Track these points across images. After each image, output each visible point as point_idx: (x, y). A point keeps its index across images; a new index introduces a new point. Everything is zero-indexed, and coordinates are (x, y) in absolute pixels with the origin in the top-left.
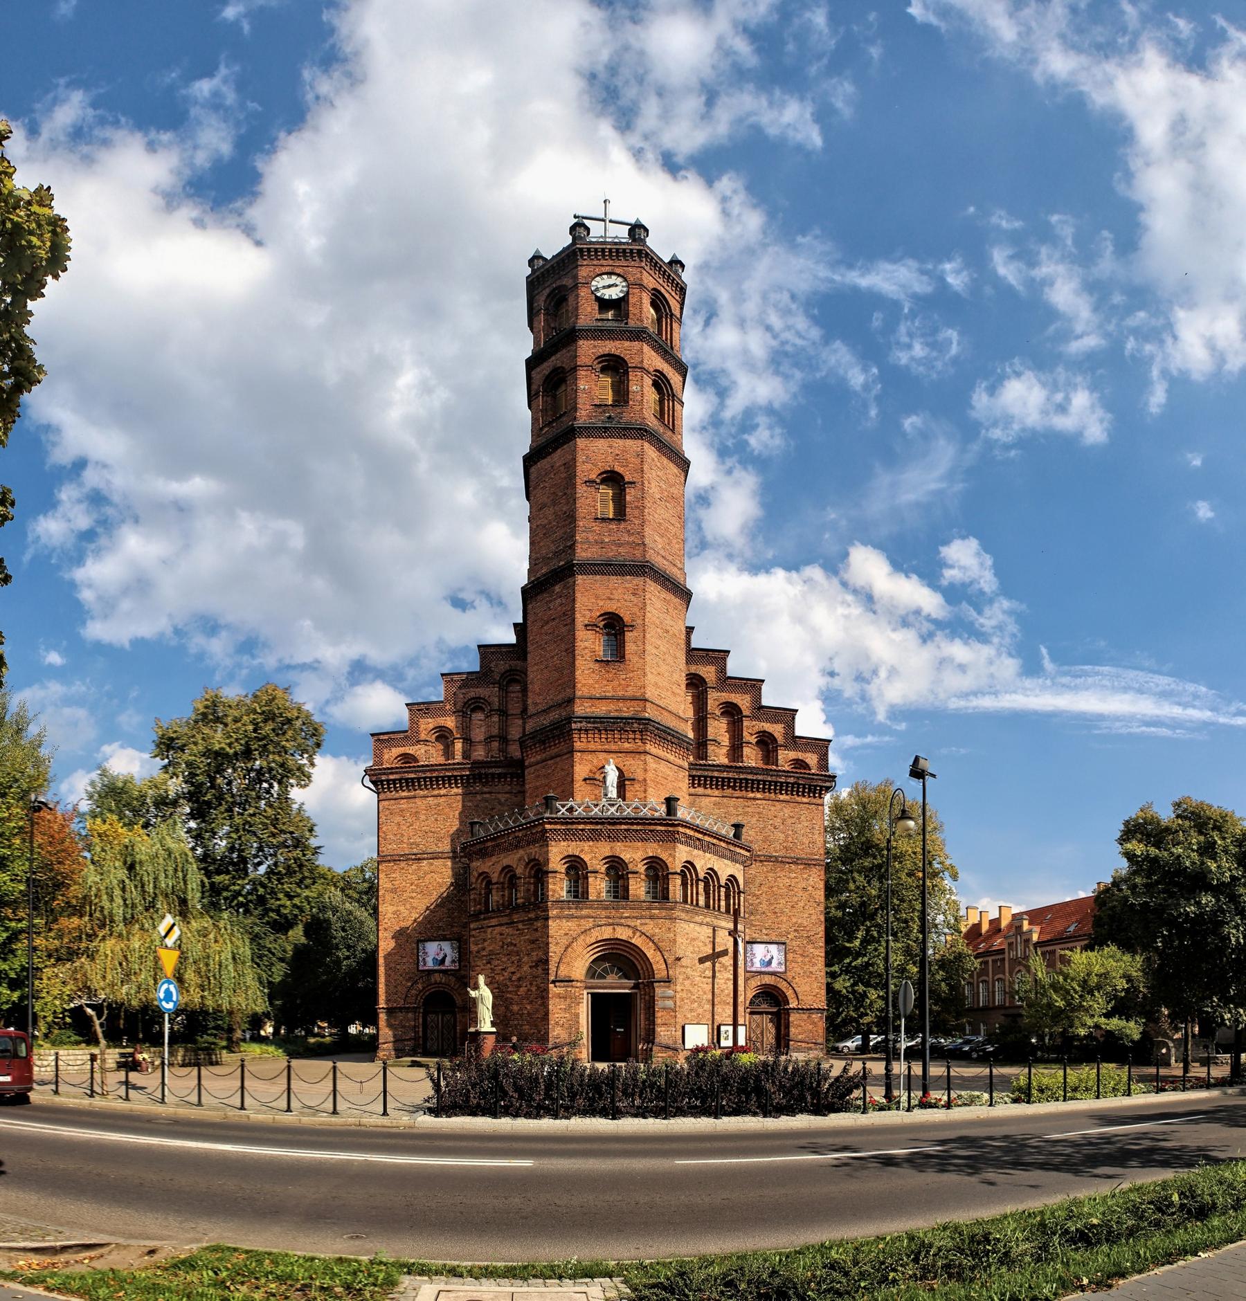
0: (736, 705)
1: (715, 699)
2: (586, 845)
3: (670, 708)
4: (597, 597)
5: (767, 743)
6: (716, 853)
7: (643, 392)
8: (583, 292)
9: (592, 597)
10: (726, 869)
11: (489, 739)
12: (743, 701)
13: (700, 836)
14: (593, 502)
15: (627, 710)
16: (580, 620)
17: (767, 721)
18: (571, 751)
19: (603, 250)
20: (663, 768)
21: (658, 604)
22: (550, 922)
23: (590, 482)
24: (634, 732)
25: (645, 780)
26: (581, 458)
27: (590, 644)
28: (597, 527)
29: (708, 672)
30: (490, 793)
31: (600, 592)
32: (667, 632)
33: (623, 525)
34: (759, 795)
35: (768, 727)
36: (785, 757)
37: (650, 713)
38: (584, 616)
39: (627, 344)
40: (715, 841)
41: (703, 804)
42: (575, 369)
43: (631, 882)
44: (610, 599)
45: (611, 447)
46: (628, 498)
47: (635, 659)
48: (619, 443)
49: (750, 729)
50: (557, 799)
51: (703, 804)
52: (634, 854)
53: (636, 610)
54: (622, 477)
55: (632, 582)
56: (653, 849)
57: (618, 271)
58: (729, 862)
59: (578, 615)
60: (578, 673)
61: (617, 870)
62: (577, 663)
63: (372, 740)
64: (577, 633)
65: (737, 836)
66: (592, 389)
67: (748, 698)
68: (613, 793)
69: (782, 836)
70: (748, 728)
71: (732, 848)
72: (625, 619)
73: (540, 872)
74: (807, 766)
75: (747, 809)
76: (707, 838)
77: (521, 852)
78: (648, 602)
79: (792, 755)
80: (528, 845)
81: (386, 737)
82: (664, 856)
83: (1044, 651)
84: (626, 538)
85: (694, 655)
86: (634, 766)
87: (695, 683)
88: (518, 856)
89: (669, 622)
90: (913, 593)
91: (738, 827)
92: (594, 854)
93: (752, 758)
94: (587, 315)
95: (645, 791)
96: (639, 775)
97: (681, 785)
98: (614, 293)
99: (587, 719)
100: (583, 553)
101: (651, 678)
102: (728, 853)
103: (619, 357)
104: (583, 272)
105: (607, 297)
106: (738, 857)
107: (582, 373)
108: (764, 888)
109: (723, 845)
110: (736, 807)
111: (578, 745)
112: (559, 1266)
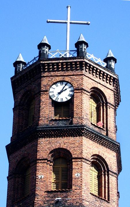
8: (44, 98)
57: (67, 79)
66: (46, 177)
94: (47, 114)
98: (65, 97)
103: (66, 150)
104: (45, 82)
105: (59, 101)
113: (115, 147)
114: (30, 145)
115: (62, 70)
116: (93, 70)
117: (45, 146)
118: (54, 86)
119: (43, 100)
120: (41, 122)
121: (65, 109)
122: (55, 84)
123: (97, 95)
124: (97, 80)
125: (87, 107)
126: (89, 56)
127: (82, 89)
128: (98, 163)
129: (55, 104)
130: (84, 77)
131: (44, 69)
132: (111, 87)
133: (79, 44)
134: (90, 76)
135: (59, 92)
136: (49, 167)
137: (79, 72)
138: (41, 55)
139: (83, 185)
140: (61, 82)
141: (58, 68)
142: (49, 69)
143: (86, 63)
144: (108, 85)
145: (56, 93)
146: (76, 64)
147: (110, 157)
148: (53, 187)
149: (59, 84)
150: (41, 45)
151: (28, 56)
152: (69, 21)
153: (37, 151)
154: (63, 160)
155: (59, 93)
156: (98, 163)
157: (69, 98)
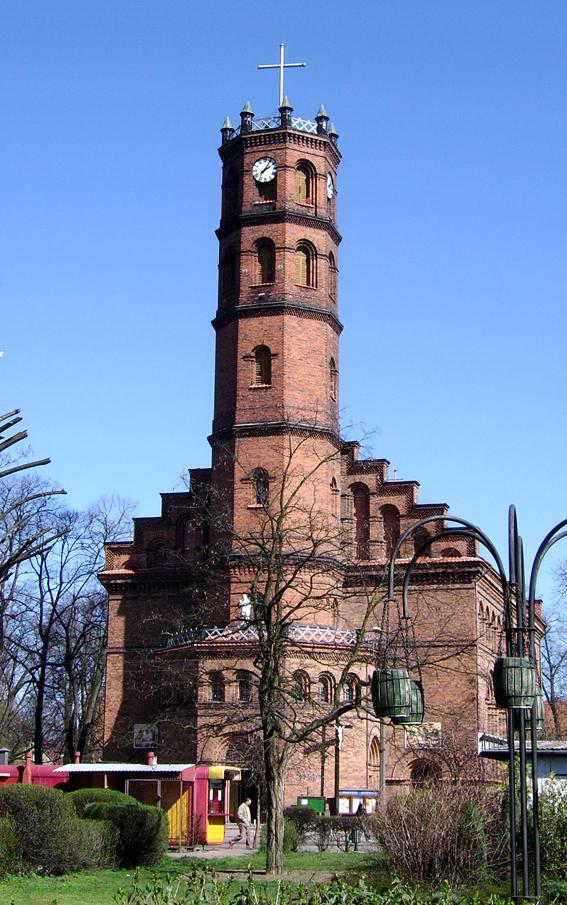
1: (376, 503)
5: (423, 545)
7: (292, 266)
8: (247, 179)
14: (248, 373)
16: (239, 474)
22: (198, 719)
23: (247, 357)
28: (251, 395)
29: (370, 480)
39: (275, 226)
44: (259, 457)
45: (261, 323)
48: (267, 320)
49: (407, 525)
50: (206, 628)
55: (274, 440)
57: (270, 154)
66: (251, 270)
67: (403, 497)
70: (404, 525)
79: (443, 545)
83: (131, 572)
85: (354, 467)
87: (360, 492)
90: (45, 620)
94: (252, 198)
98: (268, 176)
103: (269, 238)
104: (247, 159)
105: (263, 181)
112: (178, 838)
113: (328, 226)
114: (234, 234)
115: (265, 144)
116: (298, 138)
117: (249, 235)
118: (257, 163)
119: (246, 181)
120: (244, 209)
121: (269, 189)
122: (258, 160)
123: (305, 166)
124: (305, 149)
125: (294, 181)
126: (300, 124)
127: (286, 166)
128: (306, 247)
129: (259, 184)
130: (288, 151)
131: (246, 144)
132: (322, 153)
133: (283, 110)
134: (296, 147)
135: (263, 171)
136: (255, 258)
137: (281, 145)
138: (244, 126)
139: (287, 277)
140: (265, 158)
141: (260, 142)
142: (251, 143)
143: (290, 134)
144: (318, 152)
145: (259, 172)
146: (278, 137)
147: (319, 238)
148: (258, 283)
149: (262, 161)
150: (244, 115)
151: (233, 123)
152: (282, 65)
153: (240, 242)
154: (267, 250)
155: (262, 172)
156: (306, 247)
157: (273, 177)
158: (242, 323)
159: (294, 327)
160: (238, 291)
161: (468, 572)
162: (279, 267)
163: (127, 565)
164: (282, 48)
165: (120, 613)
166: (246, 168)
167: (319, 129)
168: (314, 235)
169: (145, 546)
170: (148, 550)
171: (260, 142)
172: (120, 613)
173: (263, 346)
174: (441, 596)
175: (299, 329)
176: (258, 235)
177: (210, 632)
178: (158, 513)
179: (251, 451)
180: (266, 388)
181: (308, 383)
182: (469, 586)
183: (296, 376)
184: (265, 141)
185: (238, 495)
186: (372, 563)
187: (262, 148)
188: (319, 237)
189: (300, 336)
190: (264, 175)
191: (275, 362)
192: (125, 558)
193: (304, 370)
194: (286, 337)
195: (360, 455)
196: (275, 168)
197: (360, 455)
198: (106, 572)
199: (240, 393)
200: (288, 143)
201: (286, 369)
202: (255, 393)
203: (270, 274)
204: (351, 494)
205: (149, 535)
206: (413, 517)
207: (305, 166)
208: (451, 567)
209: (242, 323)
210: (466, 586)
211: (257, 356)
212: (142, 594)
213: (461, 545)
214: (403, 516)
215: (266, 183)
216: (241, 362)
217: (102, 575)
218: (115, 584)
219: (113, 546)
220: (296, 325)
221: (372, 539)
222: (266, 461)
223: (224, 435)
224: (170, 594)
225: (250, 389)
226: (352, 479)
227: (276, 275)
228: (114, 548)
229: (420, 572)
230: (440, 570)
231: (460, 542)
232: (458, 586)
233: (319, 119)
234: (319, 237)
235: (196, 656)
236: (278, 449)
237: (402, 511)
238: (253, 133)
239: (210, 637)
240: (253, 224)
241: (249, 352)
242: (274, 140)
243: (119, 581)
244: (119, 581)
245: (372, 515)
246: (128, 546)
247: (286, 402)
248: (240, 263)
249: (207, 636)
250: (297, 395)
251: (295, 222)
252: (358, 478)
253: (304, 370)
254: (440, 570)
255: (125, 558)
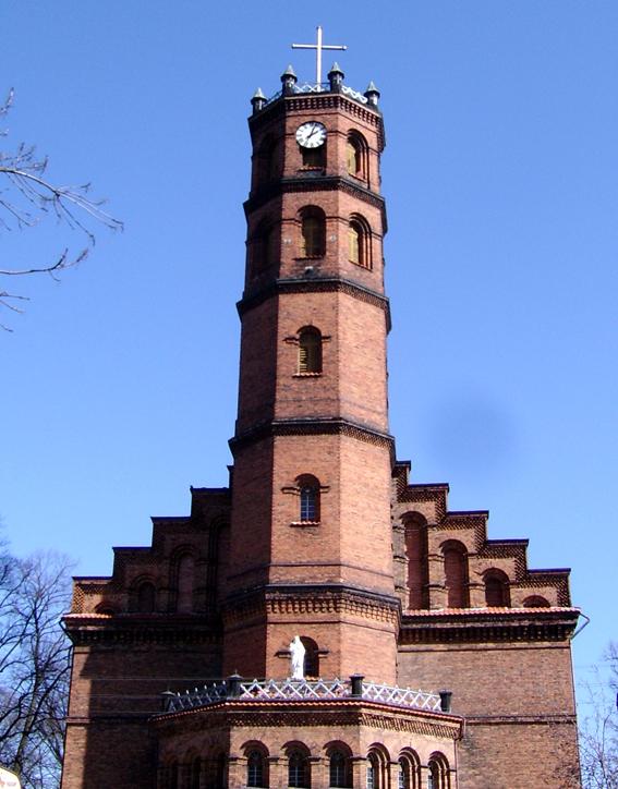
0: (459, 542)
1: (435, 538)
2: (269, 730)
3: (371, 567)
4: (294, 458)
5: (497, 587)
6: (413, 730)
7: (344, 240)
8: (289, 143)
9: (290, 458)
10: (425, 746)
11: (198, 590)
12: (467, 537)
13: (390, 715)
14: (291, 359)
15: (321, 578)
16: (278, 483)
17: (494, 556)
18: (265, 622)
19: (306, 100)
20: (361, 634)
21: (355, 458)
23: (289, 339)
24: (328, 602)
25: (339, 652)
26: (282, 315)
27: (286, 507)
28: (295, 384)
29: (428, 509)
30: (193, 652)
31: (297, 454)
32: (367, 485)
33: (320, 380)
34: (491, 645)
35: (497, 563)
36: (518, 594)
37: (345, 578)
38: (282, 478)
39: (325, 193)
40: (410, 718)
41: (426, 661)
42: (280, 221)
43: (313, 769)
44: (306, 460)
46: (324, 353)
47: (330, 521)
48: (316, 297)
49: (476, 568)
50: (241, 681)
51: (426, 661)
52: (316, 738)
53: (330, 470)
54: (319, 331)
55: (326, 440)
56: (336, 733)
57: (318, 119)
58: (433, 738)
59: (275, 478)
60: (274, 538)
61: (299, 757)
62: (274, 528)
63: (73, 583)
64: (274, 496)
65: (444, 705)
66: (293, 241)
68: (299, 673)
69: (521, 691)
71: (433, 722)
72: (321, 481)
73: (223, 760)
74: (544, 603)
75: (479, 663)
76: (398, 716)
77: (206, 734)
78: (342, 459)
79: (527, 592)
80: (212, 727)
81: (88, 582)
82: (348, 740)
84: (323, 395)
85: (406, 493)
86: (322, 636)
87: (414, 527)
88: (202, 738)
89: (368, 473)
91: (445, 698)
92: (275, 739)
93: (479, 605)
94: (293, 163)
95: (339, 664)
96: (333, 648)
97: (384, 649)
99: (282, 589)
100: (283, 412)
101: (347, 538)
102: (430, 729)
103: (317, 207)
104: (290, 123)
105: (309, 146)
106: (443, 731)
107: (285, 227)
108: (503, 757)
109: (421, 720)
110: (464, 661)
111: (272, 617)
113: (379, 203)
115: (312, 108)
117: (292, 203)
118: (302, 128)
120: (286, 174)
121: (316, 156)
122: (303, 125)
123: (356, 139)
124: (356, 119)
125: (344, 152)
127: (337, 131)
128: (359, 223)
129: (303, 150)
130: (340, 117)
134: (348, 114)
135: (309, 136)
136: (298, 229)
138: (286, 90)
139: (340, 250)
141: (307, 105)
143: (342, 99)
144: (369, 126)
145: (304, 137)
146: (328, 101)
147: (372, 215)
150: (285, 77)
152: (319, 46)
154: (315, 221)
155: (309, 137)
156: (359, 223)
157: (321, 143)
158: (284, 299)
159: (349, 309)
160: (278, 263)
161: (563, 626)
162: (330, 238)
163: (99, 609)
164: (320, 30)
165: (84, 674)
166: (288, 131)
167: (370, 104)
168: (368, 212)
169: (128, 583)
170: (130, 589)
171: (307, 105)
172: (84, 674)
173: (311, 327)
174: (526, 657)
175: (355, 311)
176: (307, 202)
177: (247, 687)
178: (147, 542)
179: (297, 454)
180: (316, 377)
181: (365, 376)
182: (563, 644)
183: (352, 366)
184: (312, 105)
185: (277, 509)
186: (432, 612)
187: (307, 112)
188: (372, 214)
189: (356, 320)
190: (310, 140)
191: (326, 348)
192: (97, 599)
193: (361, 361)
194: (341, 318)
195: (414, 478)
196: (324, 134)
197: (414, 478)
198: (74, 615)
199: (281, 381)
200: (339, 109)
201: (341, 355)
202: (301, 382)
203: (318, 246)
204: (403, 526)
205: (134, 570)
206: (485, 556)
207: (356, 139)
208: (539, 620)
209: (284, 299)
210: (559, 644)
211: (302, 339)
212: (120, 647)
213: (549, 593)
214: (472, 555)
215: (312, 150)
216: (282, 346)
217: (68, 618)
218: (84, 631)
219: (84, 582)
220: (352, 307)
221: (431, 583)
222: (315, 466)
223: (255, 434)
224: (158, 648)
225: (294, 377)
226: (404, 508)
227: (327, 247)
228: (85, 585)
229: (500, 624)
230: (526, 623)
231: (548, 588)
232: (546, 644)
233: (368, 94)
234: (372, 214)
235: (227, 721)
236: (333, 451)
237: (471, 549)
238: (298, 95)
239: (248, 694)
240: (298, 190)
241: (293, 333)
242: (323, 104)
243: (90, 628)
244: (90, 628)
245: (431, 552)
246: (105, 582)
247: (342, 395)
248: (281, 232)
249: (243, 692)
250: (354, 389)
251: (349, 192)
252: (412, 506)
253: (361, 361)
254: (526, 623)
255: (97, 599)
